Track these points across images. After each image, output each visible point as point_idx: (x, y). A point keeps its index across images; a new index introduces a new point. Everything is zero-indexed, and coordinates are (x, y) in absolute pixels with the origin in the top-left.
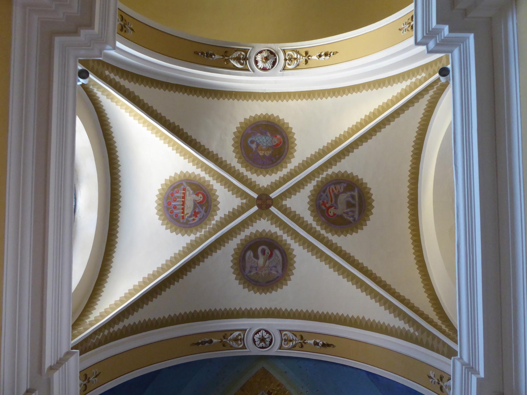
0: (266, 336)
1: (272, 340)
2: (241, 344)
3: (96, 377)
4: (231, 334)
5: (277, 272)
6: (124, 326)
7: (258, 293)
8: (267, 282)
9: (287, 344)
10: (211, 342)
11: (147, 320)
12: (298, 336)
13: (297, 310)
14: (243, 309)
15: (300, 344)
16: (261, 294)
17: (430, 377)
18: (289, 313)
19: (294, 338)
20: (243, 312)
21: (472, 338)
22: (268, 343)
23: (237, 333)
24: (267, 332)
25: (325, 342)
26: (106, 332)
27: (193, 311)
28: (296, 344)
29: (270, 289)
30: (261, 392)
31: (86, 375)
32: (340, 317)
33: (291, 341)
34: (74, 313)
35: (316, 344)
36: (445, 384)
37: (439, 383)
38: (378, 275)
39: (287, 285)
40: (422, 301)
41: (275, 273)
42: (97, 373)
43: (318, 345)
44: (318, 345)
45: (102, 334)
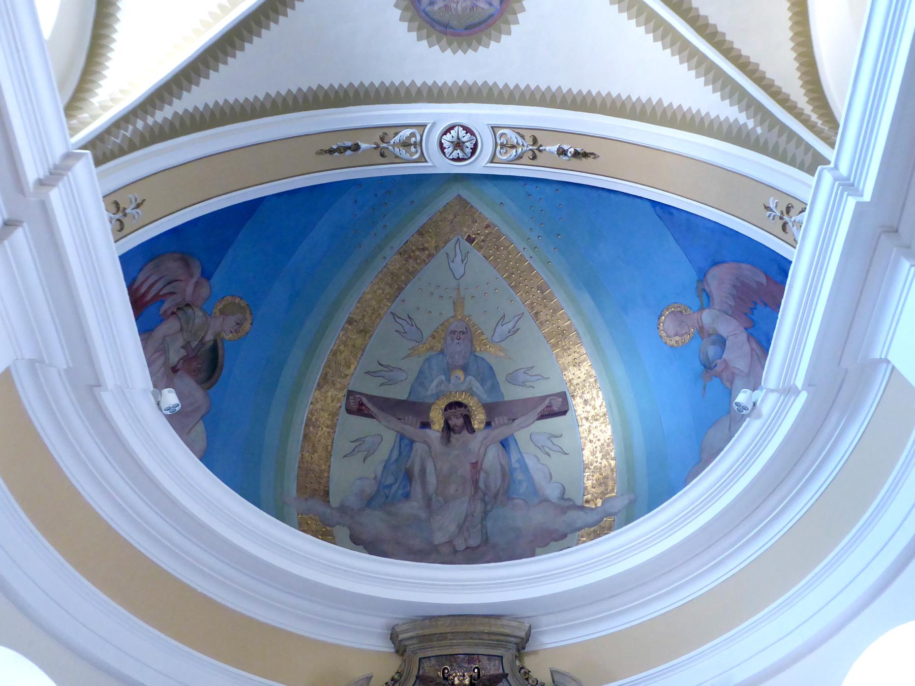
0: (466, 137)
1: (476, 145)
2: (417, 152)
3: (138, 206)
4: (396, 134)
5: (490, 4)
6: (176, 114)
7: (449, 51)
8: (468, 28)
9: (506, 153)
10: (356, 147)
11: (221, 103)
12: (527, 138)
13: (528, 87)
14: (419, 84)
15: (530, 154)
16: (454, 52)
17: (767, 208)
18: (512, 93)
19: (520, 140)
20: (419, 90)
21: (866, 132)
22: (468, 151)
23: (407, 132)
24: (467, 130)
25: (579, 149)
26: (140, 124)
27: (314, 87)
28: (523, 153)
29: (474, 42)
30: (456, 238)
31: (117, 204)
32: (614, 101)
33: (513, 147)
34: (62, 86)
35: (562, 152)
36: (793, 219)
37: (781, 218)
38: (702, 12)
39: (509, 33)
40: (784, 70)
41: (486, 7)
42: (139, 201)
43: (566, 155)
44: (566, 155)
45: (131, 127)
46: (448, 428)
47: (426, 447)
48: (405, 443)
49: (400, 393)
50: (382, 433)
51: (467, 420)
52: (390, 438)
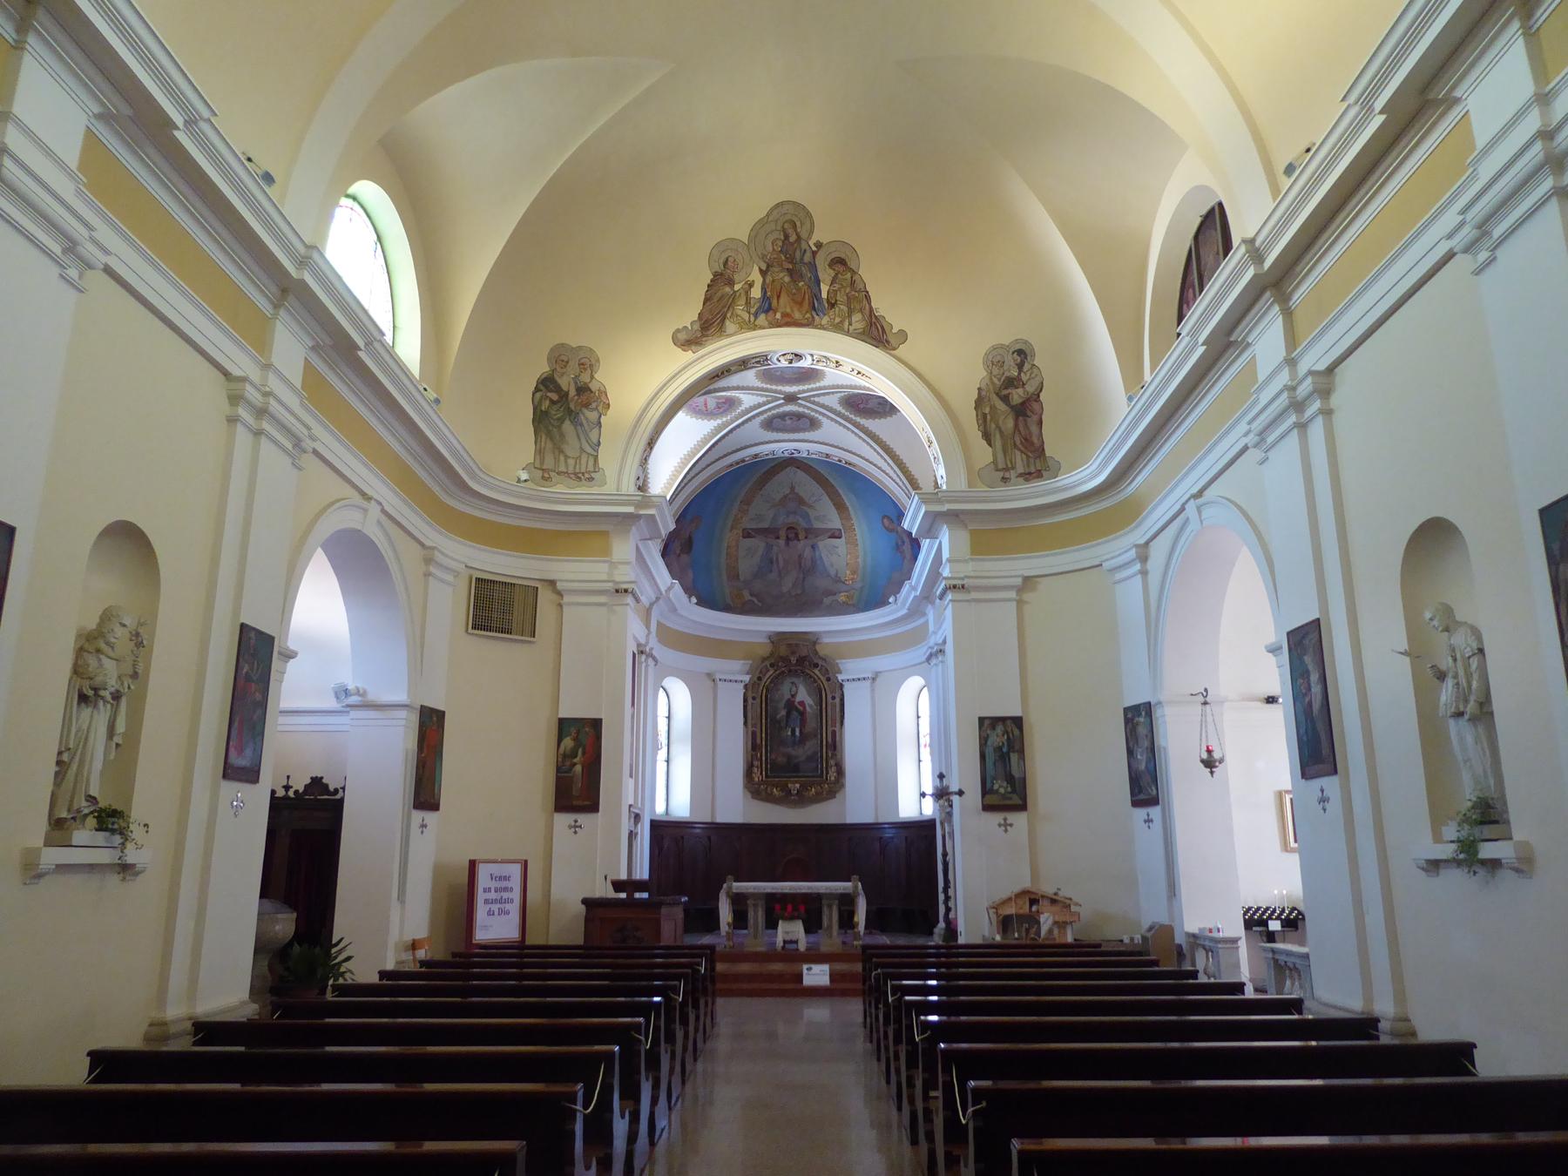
46: (788, 539)
47: (749, 377)
48: (769, 547)
49: (766, 525)
50: (758, 544)
51: (797, 536)
52: (763, 545)
